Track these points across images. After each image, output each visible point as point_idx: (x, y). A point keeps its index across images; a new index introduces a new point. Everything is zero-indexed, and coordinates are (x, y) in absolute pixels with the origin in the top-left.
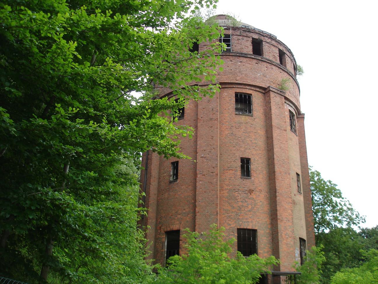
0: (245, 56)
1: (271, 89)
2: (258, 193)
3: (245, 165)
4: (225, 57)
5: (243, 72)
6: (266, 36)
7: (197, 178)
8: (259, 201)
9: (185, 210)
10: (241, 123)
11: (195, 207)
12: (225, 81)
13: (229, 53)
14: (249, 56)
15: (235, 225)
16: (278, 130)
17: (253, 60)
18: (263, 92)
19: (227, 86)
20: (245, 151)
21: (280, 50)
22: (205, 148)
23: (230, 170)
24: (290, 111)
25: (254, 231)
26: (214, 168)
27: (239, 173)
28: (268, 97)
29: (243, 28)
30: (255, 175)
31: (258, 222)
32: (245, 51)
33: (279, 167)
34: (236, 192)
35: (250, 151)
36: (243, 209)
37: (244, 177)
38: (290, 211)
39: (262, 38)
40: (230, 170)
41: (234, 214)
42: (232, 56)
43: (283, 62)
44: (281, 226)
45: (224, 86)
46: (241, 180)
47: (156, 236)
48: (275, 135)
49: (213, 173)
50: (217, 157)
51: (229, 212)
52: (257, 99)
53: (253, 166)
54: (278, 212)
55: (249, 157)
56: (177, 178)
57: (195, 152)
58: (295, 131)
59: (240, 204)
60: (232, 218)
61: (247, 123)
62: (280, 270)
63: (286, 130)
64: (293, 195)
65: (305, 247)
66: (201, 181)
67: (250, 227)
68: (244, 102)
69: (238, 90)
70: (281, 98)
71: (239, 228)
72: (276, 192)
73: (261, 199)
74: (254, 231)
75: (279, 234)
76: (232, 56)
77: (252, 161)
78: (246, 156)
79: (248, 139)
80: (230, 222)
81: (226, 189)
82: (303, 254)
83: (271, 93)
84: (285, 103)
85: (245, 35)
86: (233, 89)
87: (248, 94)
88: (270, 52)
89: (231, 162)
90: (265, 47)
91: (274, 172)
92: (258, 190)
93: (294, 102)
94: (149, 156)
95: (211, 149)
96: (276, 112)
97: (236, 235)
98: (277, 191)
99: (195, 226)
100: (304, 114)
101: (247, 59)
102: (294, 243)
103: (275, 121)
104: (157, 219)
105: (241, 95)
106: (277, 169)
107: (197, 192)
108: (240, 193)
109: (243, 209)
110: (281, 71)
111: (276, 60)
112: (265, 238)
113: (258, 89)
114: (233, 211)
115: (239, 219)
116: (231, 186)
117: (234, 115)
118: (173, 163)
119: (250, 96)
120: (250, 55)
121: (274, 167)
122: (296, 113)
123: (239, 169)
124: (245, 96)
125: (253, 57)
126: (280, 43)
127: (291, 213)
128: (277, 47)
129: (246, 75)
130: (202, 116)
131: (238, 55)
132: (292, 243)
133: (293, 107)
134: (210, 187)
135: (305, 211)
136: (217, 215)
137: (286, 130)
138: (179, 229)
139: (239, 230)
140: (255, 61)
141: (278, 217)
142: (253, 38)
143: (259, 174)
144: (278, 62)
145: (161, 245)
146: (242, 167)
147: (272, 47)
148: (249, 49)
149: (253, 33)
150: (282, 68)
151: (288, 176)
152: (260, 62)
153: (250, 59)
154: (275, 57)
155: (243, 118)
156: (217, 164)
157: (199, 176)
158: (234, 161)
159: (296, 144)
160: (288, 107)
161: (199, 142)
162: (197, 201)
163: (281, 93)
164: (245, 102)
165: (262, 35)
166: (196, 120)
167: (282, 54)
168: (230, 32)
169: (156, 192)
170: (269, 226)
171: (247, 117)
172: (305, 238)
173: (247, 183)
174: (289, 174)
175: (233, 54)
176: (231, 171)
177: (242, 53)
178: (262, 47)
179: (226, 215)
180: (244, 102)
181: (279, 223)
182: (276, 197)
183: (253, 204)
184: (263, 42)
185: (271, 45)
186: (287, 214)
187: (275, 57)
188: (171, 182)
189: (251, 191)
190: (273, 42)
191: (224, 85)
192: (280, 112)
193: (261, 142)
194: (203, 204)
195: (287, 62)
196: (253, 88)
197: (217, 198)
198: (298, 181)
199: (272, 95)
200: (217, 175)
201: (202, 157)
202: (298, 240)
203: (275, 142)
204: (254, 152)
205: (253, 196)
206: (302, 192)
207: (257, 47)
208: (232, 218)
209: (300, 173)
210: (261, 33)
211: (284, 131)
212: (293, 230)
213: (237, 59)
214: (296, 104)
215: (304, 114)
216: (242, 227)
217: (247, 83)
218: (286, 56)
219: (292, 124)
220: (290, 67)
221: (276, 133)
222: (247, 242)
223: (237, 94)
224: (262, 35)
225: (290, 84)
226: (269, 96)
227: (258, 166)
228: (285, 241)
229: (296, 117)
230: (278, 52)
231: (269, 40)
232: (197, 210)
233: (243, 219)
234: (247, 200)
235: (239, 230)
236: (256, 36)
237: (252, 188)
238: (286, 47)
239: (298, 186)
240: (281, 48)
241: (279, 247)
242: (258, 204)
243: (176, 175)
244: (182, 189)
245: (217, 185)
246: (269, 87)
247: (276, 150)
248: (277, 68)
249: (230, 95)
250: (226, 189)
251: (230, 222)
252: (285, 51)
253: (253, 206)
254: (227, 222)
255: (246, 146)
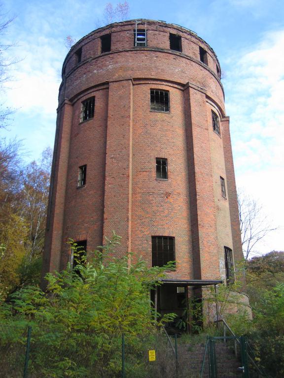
0: (162, 51)
1: (190, 85)
2: (175, 197)
3: (162, 166)
4: (138, 52)
5: (159, 67)
6: (185, 32)
7: (106, 181)
8: (177, 205)
9: (92, 217)
10: (157, 121)
11: (103, 213)
12: (139, 77)
13: (144, 48)
14: (166, 51)
15: (148, 233)
16: (199, 128)
17: (171, 55)
18: (182, 89)
19: (141, 82)
20: (161, 151)
21: (201, 48)
22: (115, 148)
23: (143, 171)
24: (213, 112)
25: (172, 239)
26: (125, 169)
27: (154, 174)
28: (187, 93)
29: (159, 23)
30: (172, 177)
31: (176, 228)
32: (161, 46)
33: (200, 167)
34: (151, 196)
35: (166, 151)
36: (158, 214)
37: (160, 179)
38: (212, 216)
39: (181, 34)
40: (143, 171)
41: (147, 220)
42: (147, 50)
43: (204, 59)
44: (202, 233)
45: (138, 82)
46: (156, 182)
47: (62, 248)
48: (195, 133)
49: (124, 175)
50: (129, 157)
51: (142, 218)
52: (175, 96)
53: (170, 168)
54: (199, 217)
55: (166, 158)
56: (85, 183)
57: (105, 120)
58: (219, 133)
59: (155, 208)
60: (145, 225)
61: (163, 120)
62: (200, 278)
63: (207, 130)
64: (216, 200)
65: (231, 258)
66: (110, 184)
67: (166, 234)
68: (160, 99)
69: (154, 87)
70: (202, 95)
71: (153, 235)
72: (196, 195)
73: (180, 204)
74: (172, 239)
75: (200, 241)
76: (147, 50)
77: (169, 161)
78: (162, 156)
79: (165, 138)
80: (143, 229)
81: (139, 193)
82: (229, 264)
83: (190, 89)
84: (207, 102)
85: (161, 29)
86: (148, 85)
87: (164, 90)
88: (190, 48)
89: (145, 163)
90: (184, 43)
91: (194, 173)
92: (176, 193)
93: (217, 102)
94: (57, 162)
95: (123, 149)
96: (196, 109)
97: (151, 243)
98: (198, 194)
99: (103, 234)
100: (228, 117)
101: (163, 54)
102: (218, 251)
103: (195, 119)
104: (63, 230)
105: (157, 93)
106: (197, 169)
107: (105, 197)
108: (156, 196)
109: (158, 214)
110: (202, 68)
111: (196, 57)
112: (184, 246)
113: (176, 86)
114: (147, 216)
115: (153, 225)
116: (144, 189)
117: (148, 112)
118: (81, 168)
119: (167, 92)
120: (168, 50)
121: (194, 168)
122: (220, 115)
123: (154, 170)
124: (162, 93)
125: (170, 52)
126: (200, 39)
127: (214, 218)
128: (197, 44)
129: (163, 70)
130: (112, 113)
131: (153, 49)
132: (215, 251)
133: (216, 107)
134: (120, 190)
135: (231, 219)
136: (128, 221)
137: (207, 130)
138: (85, 239)
139: (154, 238)
140: (173, 56)
141: (199, 223)
142: (170, 34)
143: (178, 175)
144: (199, 59)
145: (67, 258)
146: (158, 169)
147: (192, 44)
148: (166, 44)
149: (170, 28)
150: (202, 65)
151: (211, 179)
152: (179, 57)
153: (167, 54)
154: (195, 54)
155: (160, 115)
156: (128, 165)
157: (107, 179)
158: (149, 162)
159: (220, 146)
160: (210, 107)
161: (108, 142)
162: (105, 206)
163: (202, 90)
164: (162, 102)
165: (180, 31)
166: (106, 119)
167: (203, 53)
168: (145, 27)
169: (63, 201)
170: (189, 233)
171: (163, 115)
172: (232, 248)
173: (164, 185)
174: (211, 176)
175: (148, 49)
176: (145, 173)
177: (158, 48)
178: (181, 43)
179: (139, 221)
180: (160, 99)
181: (199, 229)
182: (196, 201)
183: (170, 208)
184: (182, 38)
185: (191, 42)
186: (210, 220)
187: (195, 54)
188: (78, 188)
189: (168, 195)
190: (193, 39)
191: (137, 81)
192: (201, 113)
193: (179, 141)
194: (112, 209)
195: (209, 61)
196: (170, 84)
197: (128, 202)
198: (223, 185)
199: (191, 91)
200: (129, 176)
201: (112, 158)
202: (223, 249)
203: (195, 141)
204: (171, 152)
205: (170, 200)
206: (227, 197)
207: (176, 43)
208: (145, 225)
209: (224, 177)
210: (179, 29)
211: (205, 130)
212: (217, 237)
213: (153, 54)
214: (220, 105)
215: (228, 117)
216: (157, 234)
217: (163, 79)
218: (208, 55)
219: (215, 126)
220: (212, 65)
221: (196, 132)
222: (163, 251)
223: (152, 91)
224: (180, 31)
225: (212, 84)
226: (188, 93)
227: (177, 166)
228: (207, 249)
229: (219, 119)
230: (198, 50)
231: (189, 37)
232: (105, 216)
233: (158, 225)
234: (162, 204)
235: (154, 238)
236: (174, 32)
237: (169, 191)
238: (208, 46)
239: (222, 191)
240: (203, 46)
241: (199, 256)
242: (176, 208)
243: (84, 180)
244: (89, 196)
245: (128, 188)
246: (188, 83)
247: (196, 149)
248: (198, 65)
249: (145, 91)
250: (139, 193)
251: (143, 229)
252: (206, 50)
253: (170, 211)
254: (140, 229)
255: (163, 146)
